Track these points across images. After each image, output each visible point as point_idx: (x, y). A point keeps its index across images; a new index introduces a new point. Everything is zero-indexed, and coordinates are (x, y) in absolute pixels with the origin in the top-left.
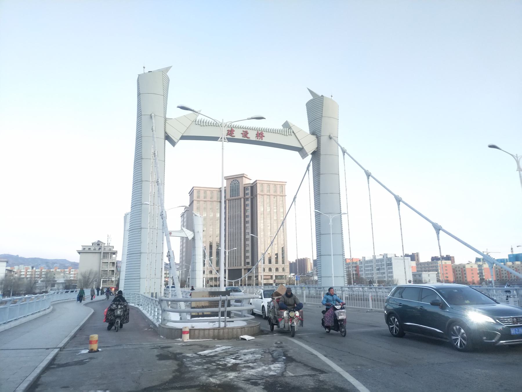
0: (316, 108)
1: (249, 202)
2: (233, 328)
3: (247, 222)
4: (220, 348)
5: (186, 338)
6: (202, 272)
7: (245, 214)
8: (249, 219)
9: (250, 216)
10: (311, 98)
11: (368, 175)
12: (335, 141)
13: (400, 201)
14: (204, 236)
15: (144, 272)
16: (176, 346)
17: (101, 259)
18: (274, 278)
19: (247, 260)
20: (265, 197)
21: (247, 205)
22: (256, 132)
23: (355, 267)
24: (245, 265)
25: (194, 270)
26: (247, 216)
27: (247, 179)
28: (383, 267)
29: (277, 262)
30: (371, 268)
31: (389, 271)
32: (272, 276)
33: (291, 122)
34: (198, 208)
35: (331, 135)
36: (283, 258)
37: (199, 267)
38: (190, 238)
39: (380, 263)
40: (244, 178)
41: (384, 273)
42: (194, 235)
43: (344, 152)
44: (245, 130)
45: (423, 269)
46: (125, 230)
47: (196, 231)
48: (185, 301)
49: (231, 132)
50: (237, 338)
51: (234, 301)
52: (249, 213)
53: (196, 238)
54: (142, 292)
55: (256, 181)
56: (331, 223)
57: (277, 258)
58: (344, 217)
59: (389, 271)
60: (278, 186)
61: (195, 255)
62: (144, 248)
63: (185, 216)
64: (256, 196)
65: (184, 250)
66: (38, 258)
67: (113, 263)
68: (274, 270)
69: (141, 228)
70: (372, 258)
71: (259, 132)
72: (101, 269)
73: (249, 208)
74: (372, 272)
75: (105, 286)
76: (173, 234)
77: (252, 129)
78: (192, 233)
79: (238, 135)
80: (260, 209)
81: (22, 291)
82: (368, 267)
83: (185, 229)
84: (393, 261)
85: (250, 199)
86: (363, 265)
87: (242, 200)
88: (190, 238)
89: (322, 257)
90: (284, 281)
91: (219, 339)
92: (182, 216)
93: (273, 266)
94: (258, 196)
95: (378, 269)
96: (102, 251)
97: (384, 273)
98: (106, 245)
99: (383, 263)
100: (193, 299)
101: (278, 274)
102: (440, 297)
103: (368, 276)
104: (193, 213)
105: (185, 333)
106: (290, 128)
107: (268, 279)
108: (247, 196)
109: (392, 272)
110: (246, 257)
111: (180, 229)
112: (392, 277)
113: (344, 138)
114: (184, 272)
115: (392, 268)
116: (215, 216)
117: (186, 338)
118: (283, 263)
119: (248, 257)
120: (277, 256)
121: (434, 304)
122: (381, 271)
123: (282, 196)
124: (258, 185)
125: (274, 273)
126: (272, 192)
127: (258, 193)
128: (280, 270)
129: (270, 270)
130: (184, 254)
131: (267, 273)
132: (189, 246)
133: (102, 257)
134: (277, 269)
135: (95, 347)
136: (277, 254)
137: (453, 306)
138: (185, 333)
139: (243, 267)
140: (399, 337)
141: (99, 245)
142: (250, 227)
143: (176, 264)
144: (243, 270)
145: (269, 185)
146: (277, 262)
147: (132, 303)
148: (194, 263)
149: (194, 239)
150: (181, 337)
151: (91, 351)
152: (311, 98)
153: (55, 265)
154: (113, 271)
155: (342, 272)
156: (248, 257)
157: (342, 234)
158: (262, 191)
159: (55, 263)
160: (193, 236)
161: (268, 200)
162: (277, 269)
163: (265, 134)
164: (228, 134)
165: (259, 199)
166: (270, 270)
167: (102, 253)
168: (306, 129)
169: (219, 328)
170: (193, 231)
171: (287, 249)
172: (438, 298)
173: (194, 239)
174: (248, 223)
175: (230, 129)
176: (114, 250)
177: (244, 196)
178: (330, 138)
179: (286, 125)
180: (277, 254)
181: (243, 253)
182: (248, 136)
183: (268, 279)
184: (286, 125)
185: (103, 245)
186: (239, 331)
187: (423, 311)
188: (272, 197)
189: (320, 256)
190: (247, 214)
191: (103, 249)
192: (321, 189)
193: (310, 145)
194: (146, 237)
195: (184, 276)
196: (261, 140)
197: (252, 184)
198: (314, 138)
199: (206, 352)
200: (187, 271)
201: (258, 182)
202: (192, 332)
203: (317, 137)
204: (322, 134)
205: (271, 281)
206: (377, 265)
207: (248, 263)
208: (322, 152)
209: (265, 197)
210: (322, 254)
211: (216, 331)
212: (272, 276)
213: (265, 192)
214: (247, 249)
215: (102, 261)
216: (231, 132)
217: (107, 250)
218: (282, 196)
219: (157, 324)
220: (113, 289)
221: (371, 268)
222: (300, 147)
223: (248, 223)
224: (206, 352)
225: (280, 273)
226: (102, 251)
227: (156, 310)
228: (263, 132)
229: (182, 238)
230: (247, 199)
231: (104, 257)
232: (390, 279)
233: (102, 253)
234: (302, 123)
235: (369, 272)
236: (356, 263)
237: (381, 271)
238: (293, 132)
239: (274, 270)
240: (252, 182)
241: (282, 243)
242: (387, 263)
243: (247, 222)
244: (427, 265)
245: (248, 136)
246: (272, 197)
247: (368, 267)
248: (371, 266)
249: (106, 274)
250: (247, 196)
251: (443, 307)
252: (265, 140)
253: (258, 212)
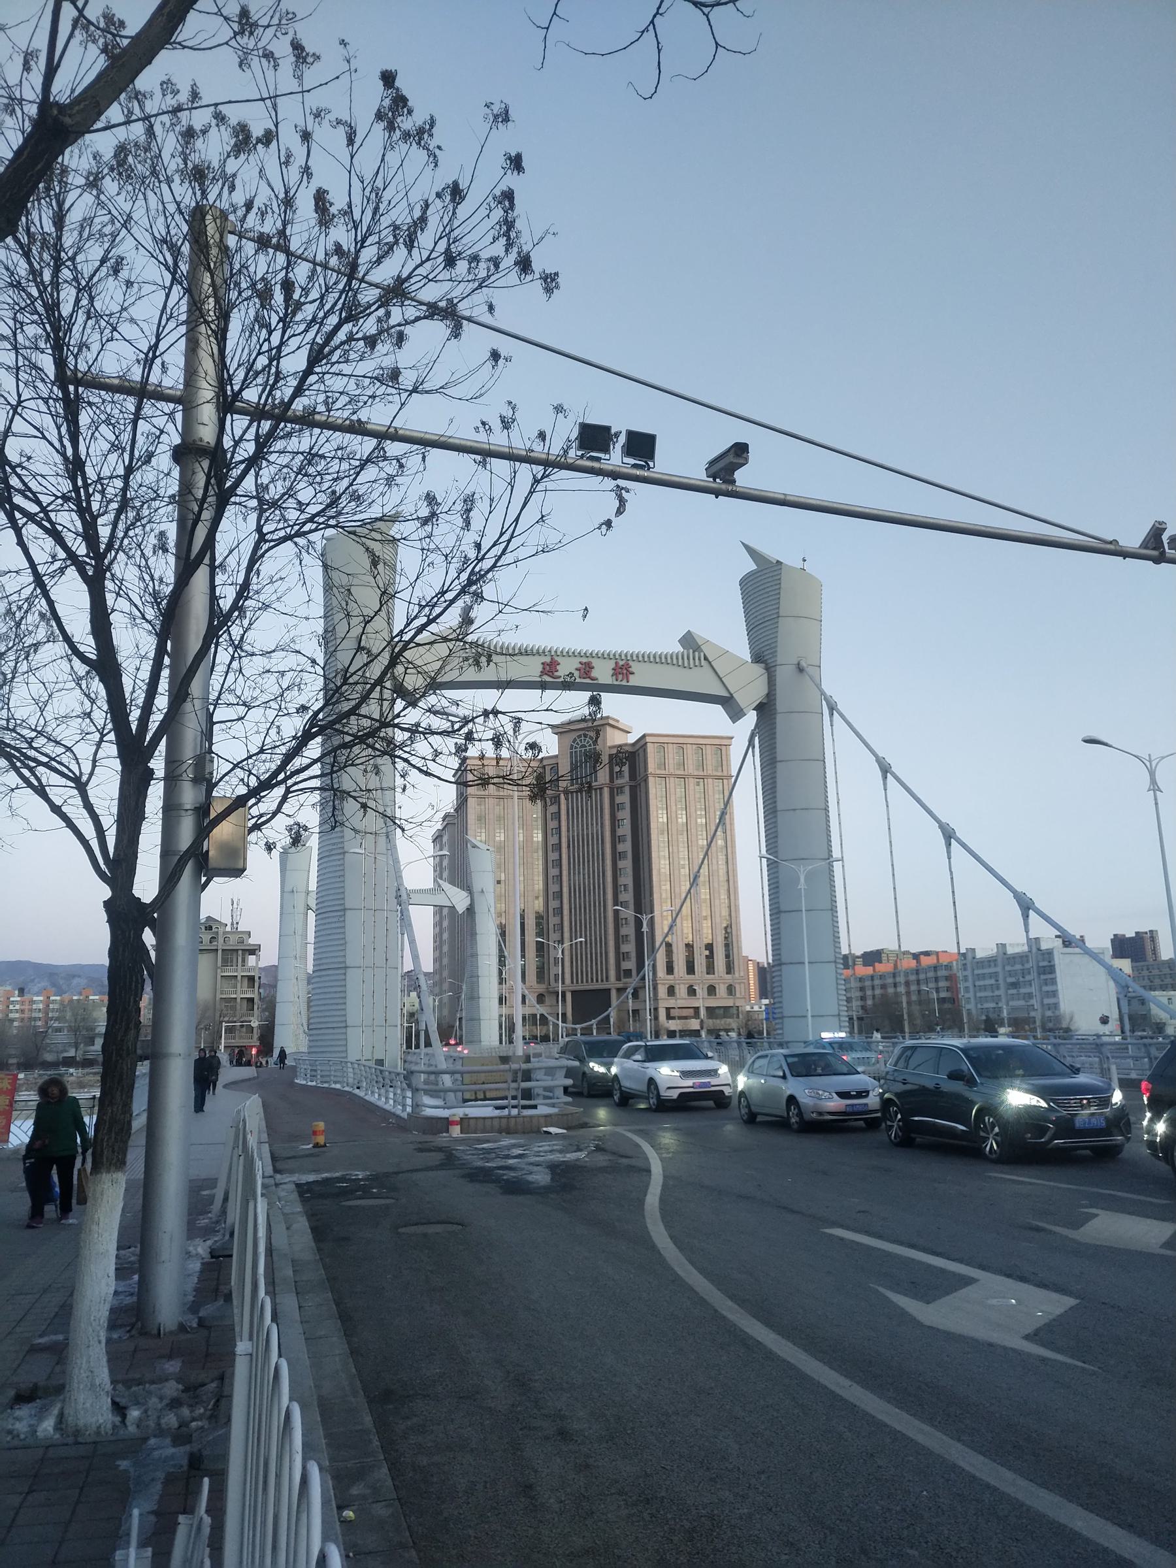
0: (766, 592)
1: (624, 798)
2: (531, 1117)
3: (622, 855)
4: (506, 1141)
5: (456, 1131)
6: (497, 1001)
7: (613, 831)
8: (626, 847)
9: (629, 838)
10: (752, 566)
11: (885, 770)
12: (811, 678)
13: (951, 838)
14: (498, 898)
15: (355, 1011)
16: (442, 1139)
17: (217, 968)
18: (703, 1012)
19: (626, 965)
20: (672, 782)
21: (620, 806)
22: (612, 664)
23: (947, 978)
24: (618, 979)
25: (474, 997)
26: (622, 839)
27: (617, 732)
28: (1028, 978)
29: (710, 969)
30: (992, 981)
31: (1045, 988)
32: (697, 1009)
33: (702, 632)
34: (480, 818)
35: (803, 664)
36: (727, 956)
37: (489, 987)
38: (461, 908)
39: (1018, 967)
40: (608, 729)
41: (1030, 996)
42: (472, 900)
43: (832, 708)
44: (584, 660)
45: (1157, 982)
46: (282, 892)
47: (476, 888)
48: (452, 1073)
49: (550, 667)
50: (538, 1131)
51: (563, 1072)
52: (625, 829)
53: (477, 909)
54: (352, 1057)
55: (644, 736)
56: (802, 885)
57: (710, 957)
58: (837, 866)
59: (1045, 988)
60: (709, 751)
61: (474, 955)
62: (353, 957)
63: (445, 839)
64: (646, 781)
65: (445, 936)
66: (29, 963)
67: (251, 979)
68: (701, 992)
69: (345, 910)
70: (1026, 948)
71: (621, 663)
72: (219, 996)
73: (625, 815)
74: (997, 993)
75: (234, 1042)
76: (415, 898)
77: (603, 656)
78: (464, 894)
79: (566, 668)
80: (658, 817)
81: (10, 1056)
82: (983, 977)
83: (446, 885)
84: (1059, 961)
85: (627, 789)
86: (968, 973)
87: (606, 791)
88: (461, 908)
89: (784, 967)
90: (733, 1023)
91: (508, 1133)
92: (437, 839)
93: (701, 976)
94: (651, 780)
95: (1014, 985)
96: (220, 944)
97: (1030, 996)
98: (228, 929)
99: (1027, 966)
100: (465, 1069)
101: (713, 1003)
102: (967, 1066)
103: (986, 1005)
104: (467, 841)
105: (454, 1123)
106: (697, 648)
107: (686, 1018)
108: (619, 782)
109: (1054, 994)
110: (621, 957)
111: (430, 885)
112: (1056, 1006)
113: (837, 674)
114: (446, 1000)
115: (1054, 982)
116: (529, 838)
117: (456, 1131)
118: (729, 972)
119: (626, 956)
120: (712, 952)
121: (955, 1076)
122: (1022, 991)
123: (721, 778)
124: (650, 747)
125: (702, 1001)
126: (691, 768)
127: (650, 770)
128: (722, 990)
129: (692, 991)
130: (445, 948)
131: (682, 999)
132: (457, 931)
133: (219, 964)
134: (712, 990)
135: (321, 1139)
136: (709, 947)
137: (984, 1080)
138: (454, 1123)
139: (613, 983)
140: (1003, 1163)
141: (211, 928)
142: (630, 871)
143: (426, 974)
144: (614, 993)
145: (681, 746)
146: (710, 969)
147: (335, 1082)
148: (475, 977)
149: (470, 910)
150: (447, 1131)
151: (316, 1146)
152: (752, 566)
153: (75, 981)
154: (251, 1000)
155: (833, 1002)
156: (626, 956)
157: (833, 909)
158: (663, 765)
159: (74, 976)
160: (467, 902)
161: (680, 791)
162: (712, 990)
163: (634, 667)
164: (543, 673)
165: (655, 788)
166: (692, 991)
167: (220, 952)
168: (742, 649)
169: (509, 1117)
170: (468, 889)
171: (738, 929)
172: (964, 1068)
173: (470, 910)
174: (625, 857)
175: (548, 659)
176: (252, 941)
177: (612, 780)
178: (800, 669)
179: (688, 640)
180: (709, 947)
181: (611, 943)
182: (594, 674)
183: (686, 1018)
184: (688, 640)
185: (221, 930)
186: (542, 1120)
187: (937, 1092)
188: (692, 782)
189: (780, 965)
190: (620, 832)
191: (221, 940)
192: (779, 799)
193: (751, 691)
194: (357, 928)
195: (446, 1012)
196: (624, 683)
197: (633, 745)
198: (759, 669)
199: (484, 1146)
200: (456, 999)
201: (648, 739)
202: (464, 1122)
203: (767, 669)
204: (780, 660)
205: (694, 1024)
206: (1010, 974)
207: (628, 973)
208: (781, 705)
209: (672, 782)
210: (784, 960)
211: (504, 1121)
212: (697, 1009)
213: (671, 768)
214: (624, 931)
215: (220, 974)
216: (550, 667)
217: (233, 942)
218: (721, 778)
219: (404, 1115)
220: (254, 1051)
221: (992, 981)
222: (726, 694)
223: (625, 857)
224: (484, 1146)
225: (722, 1000)
226: (220, 944)
227: (391, 1095)
228: (631, 663)
229: (439, 909)
230: (620, 789)
231: (225, 962)
232: (1049, 1013)
233: (220, 952)
234: (730, 636)
235: (988, 994)
236: (948, 967)
237: (1022, 991)
238: (706, 658)
239: (701, 992)
240: (631, 739)
241: (725, 913)
242: (1035, 968)
243: (622, 855)
244: (1167, 971)
245: (594, 674)
246: (692, 782)
247: (983, 977)
248: (991, 975)
249: (234, 1008)
250: (619, 782)
251: (971, 1082)
252: (634, 681)
253: (653, 825)
